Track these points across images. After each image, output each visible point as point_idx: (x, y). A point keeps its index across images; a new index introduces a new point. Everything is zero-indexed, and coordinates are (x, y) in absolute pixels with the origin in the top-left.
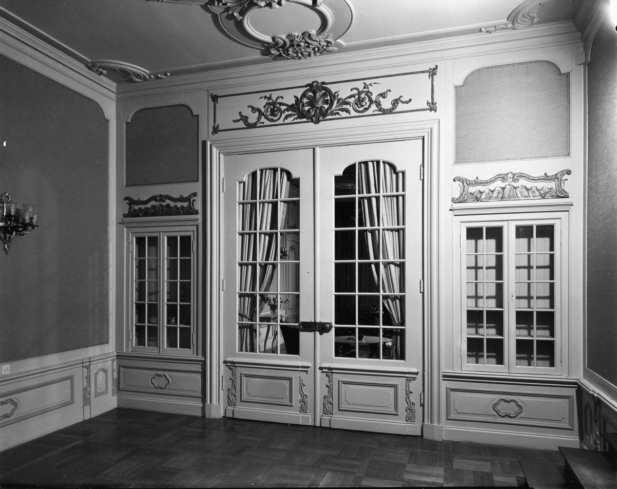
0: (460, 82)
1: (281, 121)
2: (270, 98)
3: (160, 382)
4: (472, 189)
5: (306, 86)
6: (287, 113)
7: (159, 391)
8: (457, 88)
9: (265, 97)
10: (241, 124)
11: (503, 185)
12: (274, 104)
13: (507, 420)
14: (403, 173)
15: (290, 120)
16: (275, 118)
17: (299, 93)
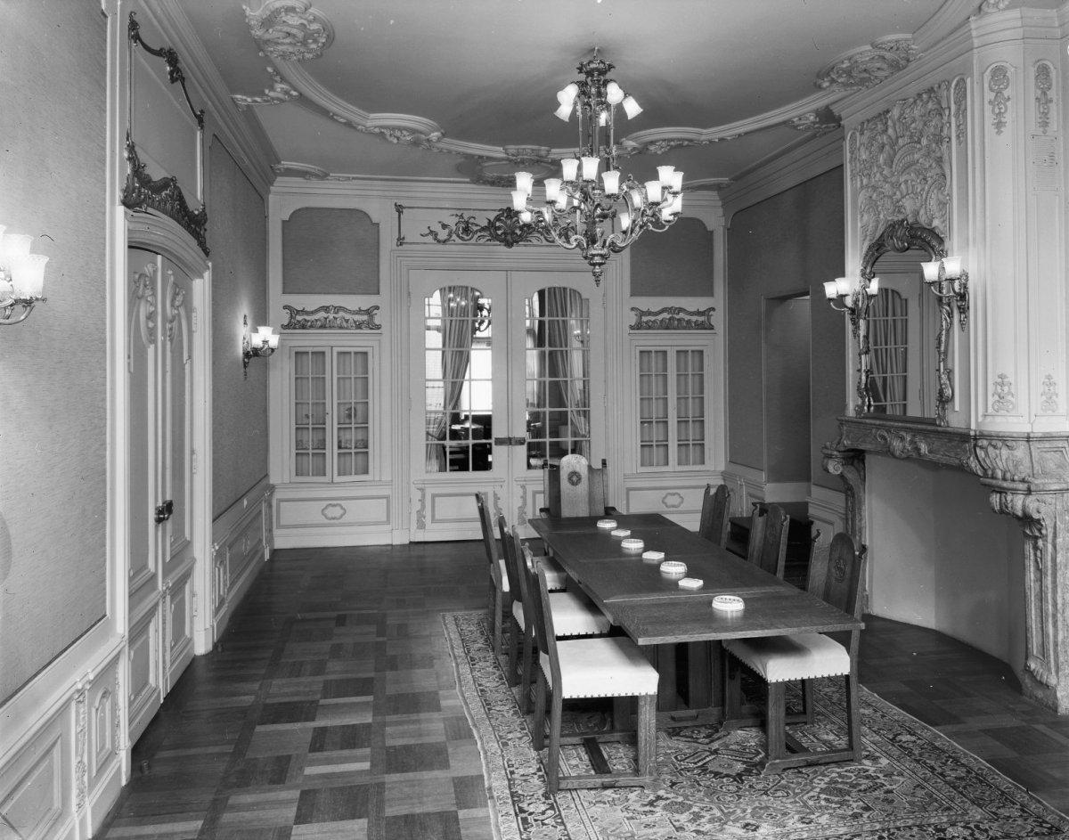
0: (286, 218)
1: (473, 241)
2: (461, 216)
3: (337, 512)
4: (299, 318)
5: (500, 210)
6: (479, 234)
7: (333, 522)
8: (284, 222)
9: (457, 215)
10: (430, 239)
11: (326, 315)
12: (467, 223)
13: (335, 502)
14: (906, 300)
15: (482, 241)
16: (466, 238)
17: (492, 216)
